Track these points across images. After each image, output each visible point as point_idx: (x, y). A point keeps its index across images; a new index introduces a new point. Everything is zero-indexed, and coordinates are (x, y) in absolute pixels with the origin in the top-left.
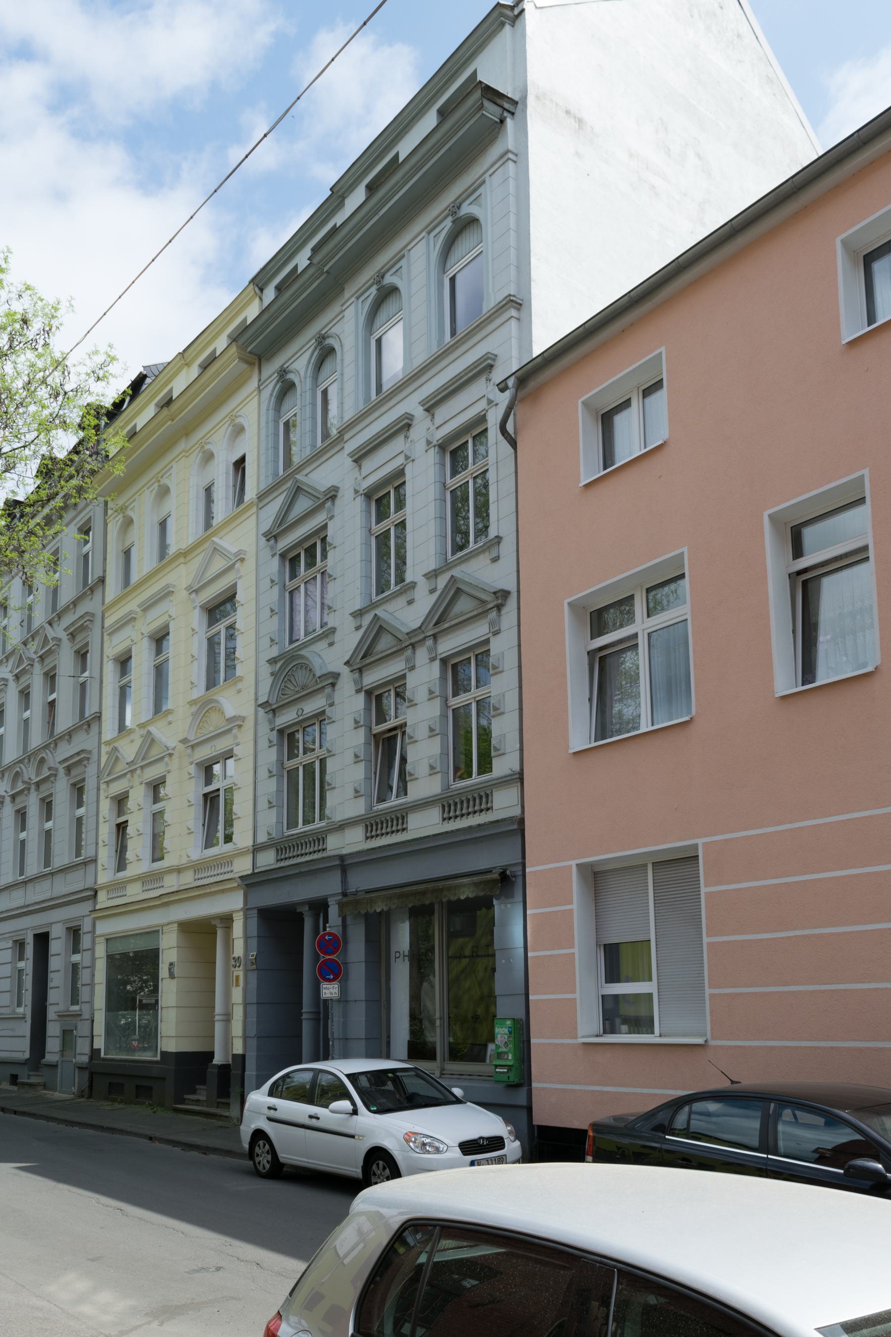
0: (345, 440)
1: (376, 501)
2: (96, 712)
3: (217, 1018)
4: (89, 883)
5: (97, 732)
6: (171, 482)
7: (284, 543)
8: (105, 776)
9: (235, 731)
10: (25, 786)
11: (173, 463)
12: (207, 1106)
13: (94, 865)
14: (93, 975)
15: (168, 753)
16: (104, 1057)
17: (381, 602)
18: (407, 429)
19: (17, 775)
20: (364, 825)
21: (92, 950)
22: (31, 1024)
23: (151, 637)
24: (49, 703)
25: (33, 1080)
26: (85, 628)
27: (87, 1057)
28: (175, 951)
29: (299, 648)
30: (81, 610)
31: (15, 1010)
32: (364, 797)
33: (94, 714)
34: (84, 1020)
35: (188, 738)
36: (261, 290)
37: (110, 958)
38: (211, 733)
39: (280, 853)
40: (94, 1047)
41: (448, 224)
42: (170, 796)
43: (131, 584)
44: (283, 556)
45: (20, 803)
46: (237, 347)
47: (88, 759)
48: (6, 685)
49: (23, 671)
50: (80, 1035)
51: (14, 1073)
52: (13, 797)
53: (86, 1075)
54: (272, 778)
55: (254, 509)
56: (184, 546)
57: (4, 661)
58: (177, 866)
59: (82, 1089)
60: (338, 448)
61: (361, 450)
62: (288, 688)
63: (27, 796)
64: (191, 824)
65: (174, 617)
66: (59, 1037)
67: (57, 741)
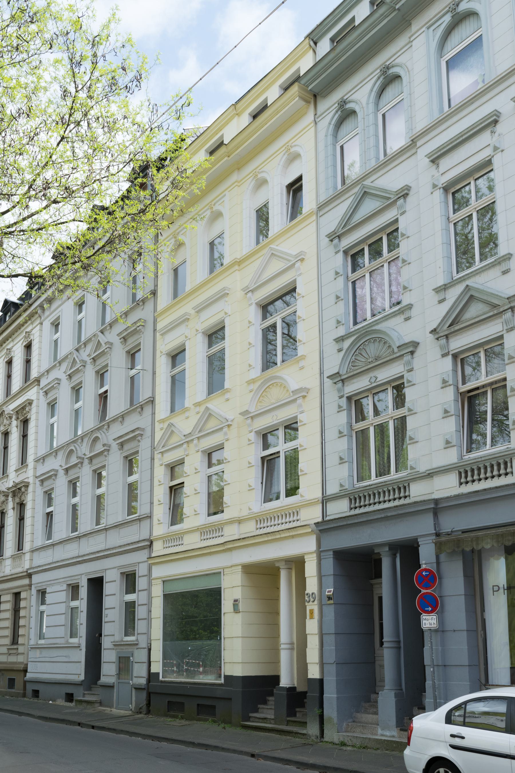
0: (418, 146)
1: (351, 256)
3: (282, 646)
4: (145, 535)
5: (151, 413)
6: (224, 208)
7: (347, 241)
8: (197, 433)
9: (300, 401)
10: (79, 460)
11: (226, 192)
12: (275, 724)
14: (150, 611)
15: (227, 424)
16: (163, 679)
17: (470, 275)
18: (494, 125)
19: (96, 439)
20: (457, 472)
21: (149, 590)
23: (168, 354)
24: (99, 395)
25: (88, 698)
26: (138, 331)
27: (145, 679)
29: (370, 325)
32: (456, 447)
34: (141, 648)
35: (249, 410)
36: (316, 43)
37: (166, 597)
38: (273, 404)
39: (203, 535)
41: (448, 18)
42: (229, 460)
43: (158, 311)
44: (346, 252)
45: (72, 475)
46: (299, 87)
47: (141, 435)
48: (85, 366)
49: (77, 371)
50: (136, 661)
52: (67, 470)
54: (342, 438)
55: (314, 217)
56: (239, 256)
57: (57, 365)
59: (140, 706)
60: (413, 151)
61: (440, 150)
62: (359, 361)
63: (54, 480)
66: (115, 662)
67: (110, 423)
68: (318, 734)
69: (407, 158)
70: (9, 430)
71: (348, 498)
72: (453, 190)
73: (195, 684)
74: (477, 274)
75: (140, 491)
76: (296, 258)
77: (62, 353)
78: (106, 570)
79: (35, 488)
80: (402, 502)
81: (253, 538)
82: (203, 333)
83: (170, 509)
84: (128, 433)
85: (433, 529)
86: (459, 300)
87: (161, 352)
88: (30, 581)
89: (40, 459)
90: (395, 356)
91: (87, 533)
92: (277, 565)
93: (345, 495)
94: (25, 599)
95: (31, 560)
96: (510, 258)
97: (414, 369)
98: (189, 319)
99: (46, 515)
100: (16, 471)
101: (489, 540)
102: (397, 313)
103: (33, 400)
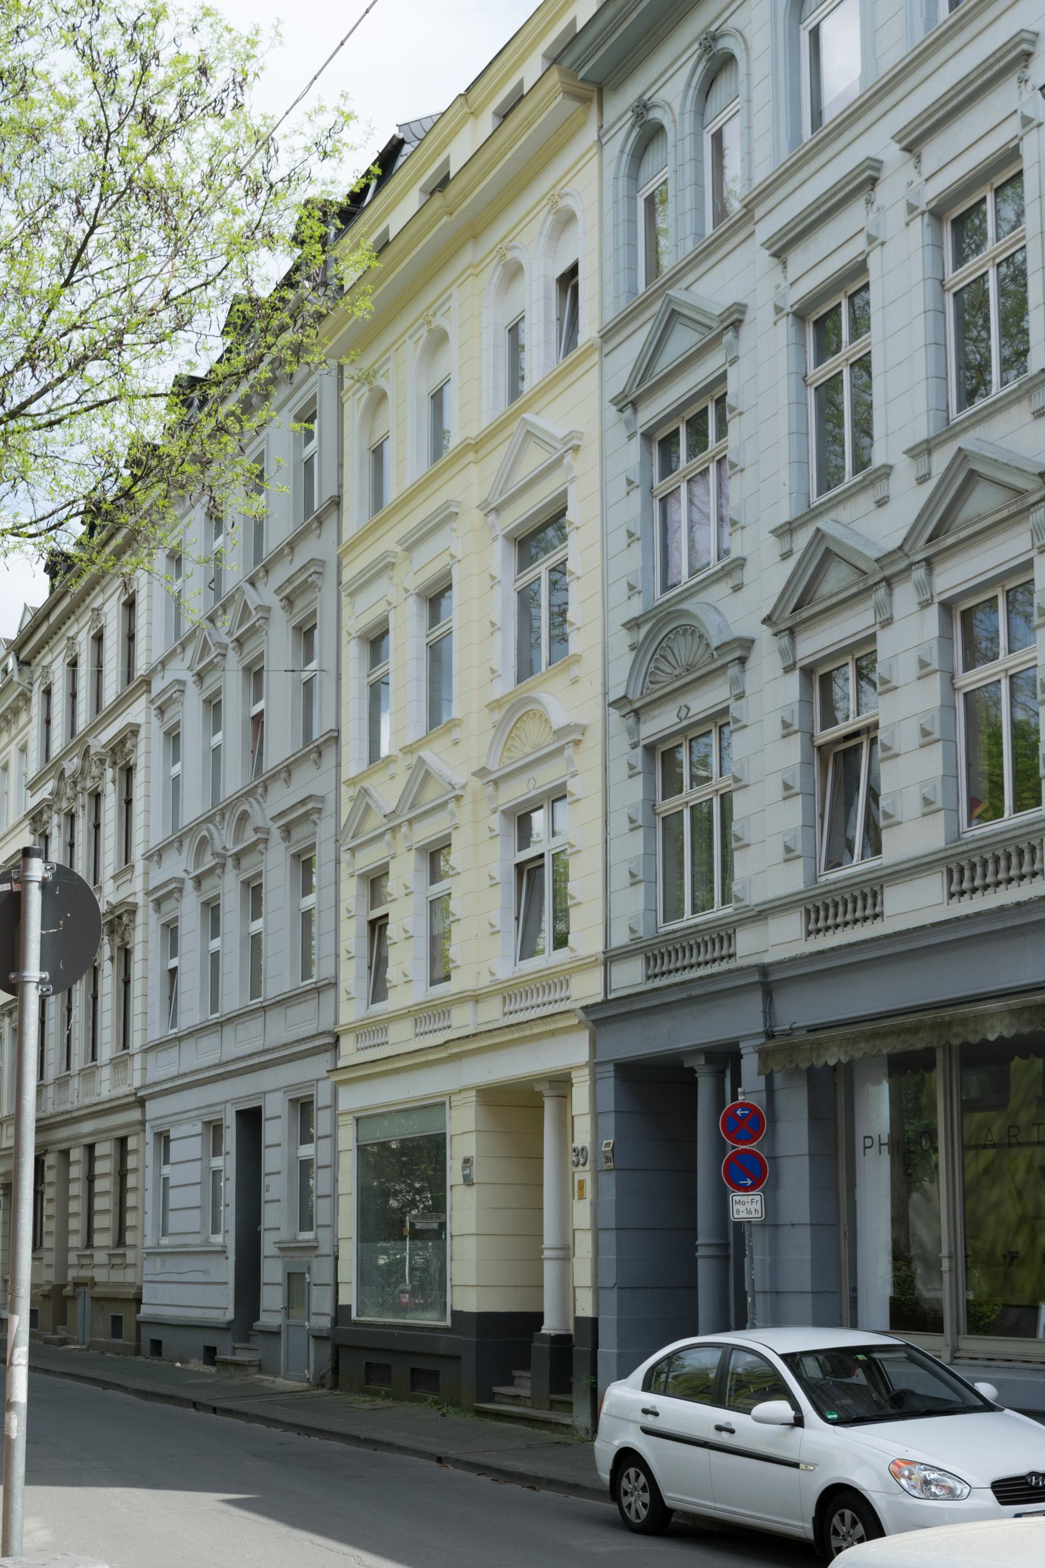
3: (547, 1254)
4: (326, 1024)
5: (334, 764)
8: (349, 840)
9: (569, 751)
10: (217, 860)
14: (336, 1180)
15: (453, 794)
17: (828, 505)
18: (870, 187)
19: (204, 842)
21: (333, 1136)
22: (236, 1262)
23: (362, 638)
24: (253, 718)
25: (241, 1357)
27: (329, 1318)
30: (302, 556)
31: (208, 1238)
32: (802, 859)
34: (323, 1256)
35: (489, 767)
37: (362, 1150)
39: (652, 963)
40: (341, 1303)
42: (459, 870)
46: (561, 73)
47: (319, 811)
48: (183, 691)
52: (198, 880)
53: (328, 1350)
55: (595, 358)
56: (474, 431)
57: (179, 651)
62: (662, 671)
63: (178, 900)
68: (589, 1426)
69: (742, 242)
70: (100, 789)
71: (643, 956)
72: (815, 317)
73: (406, 1327)
74: (839, 502)
75: (319, 929)
76: (565, 444)
77: (229, 584)
78: (265, 1093)
79: (146, 915)
80: (724, 966)
81: (489, 1034)
82: (418, 595)
83: (370, 968)
84: (294, 806)
85: (762, 1024)
86: (808, 556)
87: (349, 634)
88: (144, 1113)
89: (152, 855)
90: (714, 666)
91: (231, 1015)
92: (538, 1088)
93: (637, 949)
94: (136, 1151)
95: (144, 1069)
96: (888, 475)
97: (747, 694)
98: (394, 564)
99: (168, 974)
100: (115, 877)
101: (835, 1049)
102: (721, 574)
103: (139, 726)
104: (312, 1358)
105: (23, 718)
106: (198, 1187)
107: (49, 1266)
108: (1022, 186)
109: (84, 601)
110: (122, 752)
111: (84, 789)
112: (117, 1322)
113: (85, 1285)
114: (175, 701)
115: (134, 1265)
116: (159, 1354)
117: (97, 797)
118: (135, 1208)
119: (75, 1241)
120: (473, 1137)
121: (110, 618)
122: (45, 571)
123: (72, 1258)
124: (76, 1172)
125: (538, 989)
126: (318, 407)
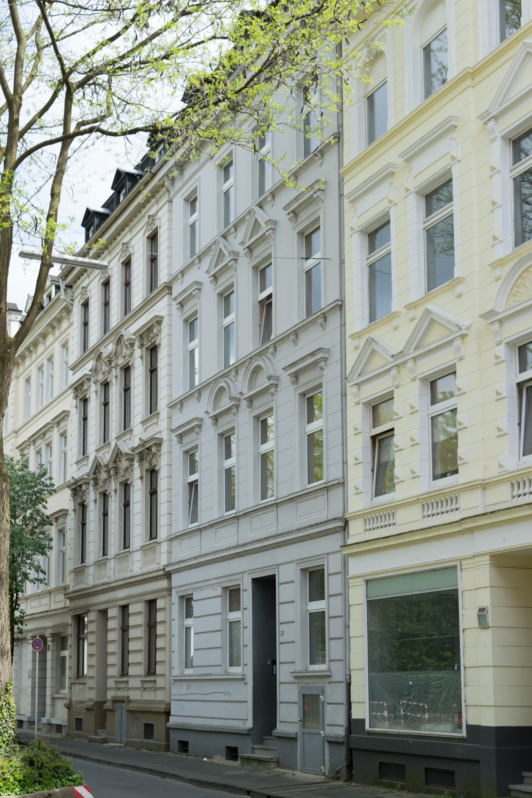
2: (337, 300)
4: (336, 511)
5: (339, 325)
10: (233, 403)
13: (341, 489)
14: (347, 627)
16: (370, 729)
21: (344, 594)
22: (254, 687)
24: (260, 302)
25: (258, 755)
26: (315, 200)
28: (487, 592)
30: (303, 184)
31: (227, 669)
33: (334, 302)
34: (336, 682)
37: (372, 604)
39: (368, 522)
40: (354, 716)
45: (224, 424)
48: (200, 290)
49: (226, 268)
51: (184, 739)
52: (216, 419)
53: (343, 752)
56: (471, 63)
58: (483, 480)
59: (337, 769)
63: (198, 434)
64: (504, 424)
65: (459, 158)
66: (297, 703)
67: (276, 345)
70: (108, 380)
78: (278, 565)
79: (170, 446)
81: (507, 511)
82: (417, 193)
84: (304, 357)
87: (352, 229)
88: (170, 583)
94: (163, 609)
98: (394, 173)
100: (143, 423)
104: (327, 758)
105: (65, 324)
106: (220, 633)
107: (91, 688)
108: (452, 188)
109: (115, 239)
110: (81, 390)
111: (117, 365)
112: (149, 729)
113: (123, 702)
114: (194, 297)
115: (164, 688)
116: (186, 751)
117: (127, 370)
118: (164, 649)
119: (113, 671)
120: (488, 591)
121: (93, 292)
122: (82, 225)
123: (111, 683)
124: (113, 624)
125: (442, 502)
126: (198, 194)
